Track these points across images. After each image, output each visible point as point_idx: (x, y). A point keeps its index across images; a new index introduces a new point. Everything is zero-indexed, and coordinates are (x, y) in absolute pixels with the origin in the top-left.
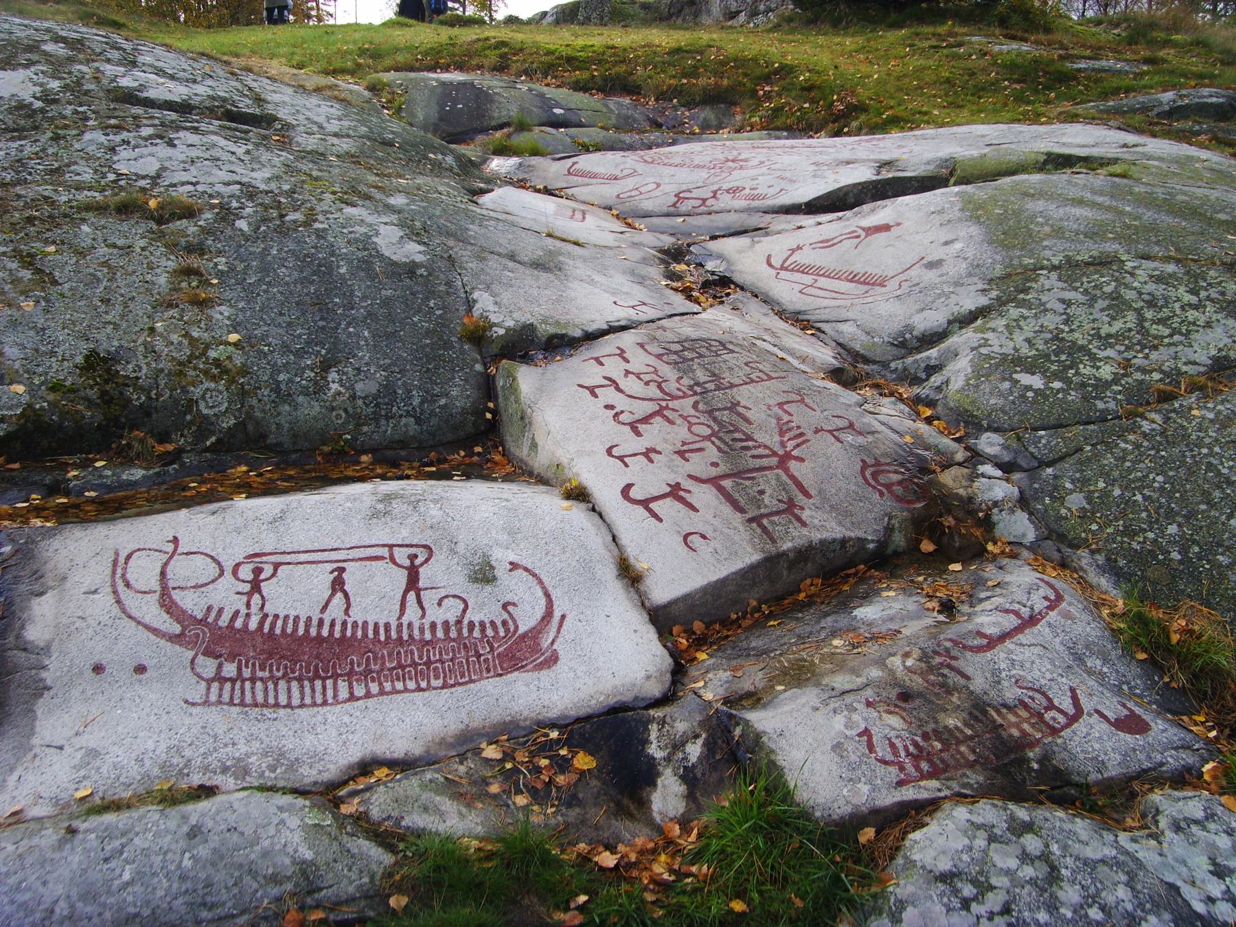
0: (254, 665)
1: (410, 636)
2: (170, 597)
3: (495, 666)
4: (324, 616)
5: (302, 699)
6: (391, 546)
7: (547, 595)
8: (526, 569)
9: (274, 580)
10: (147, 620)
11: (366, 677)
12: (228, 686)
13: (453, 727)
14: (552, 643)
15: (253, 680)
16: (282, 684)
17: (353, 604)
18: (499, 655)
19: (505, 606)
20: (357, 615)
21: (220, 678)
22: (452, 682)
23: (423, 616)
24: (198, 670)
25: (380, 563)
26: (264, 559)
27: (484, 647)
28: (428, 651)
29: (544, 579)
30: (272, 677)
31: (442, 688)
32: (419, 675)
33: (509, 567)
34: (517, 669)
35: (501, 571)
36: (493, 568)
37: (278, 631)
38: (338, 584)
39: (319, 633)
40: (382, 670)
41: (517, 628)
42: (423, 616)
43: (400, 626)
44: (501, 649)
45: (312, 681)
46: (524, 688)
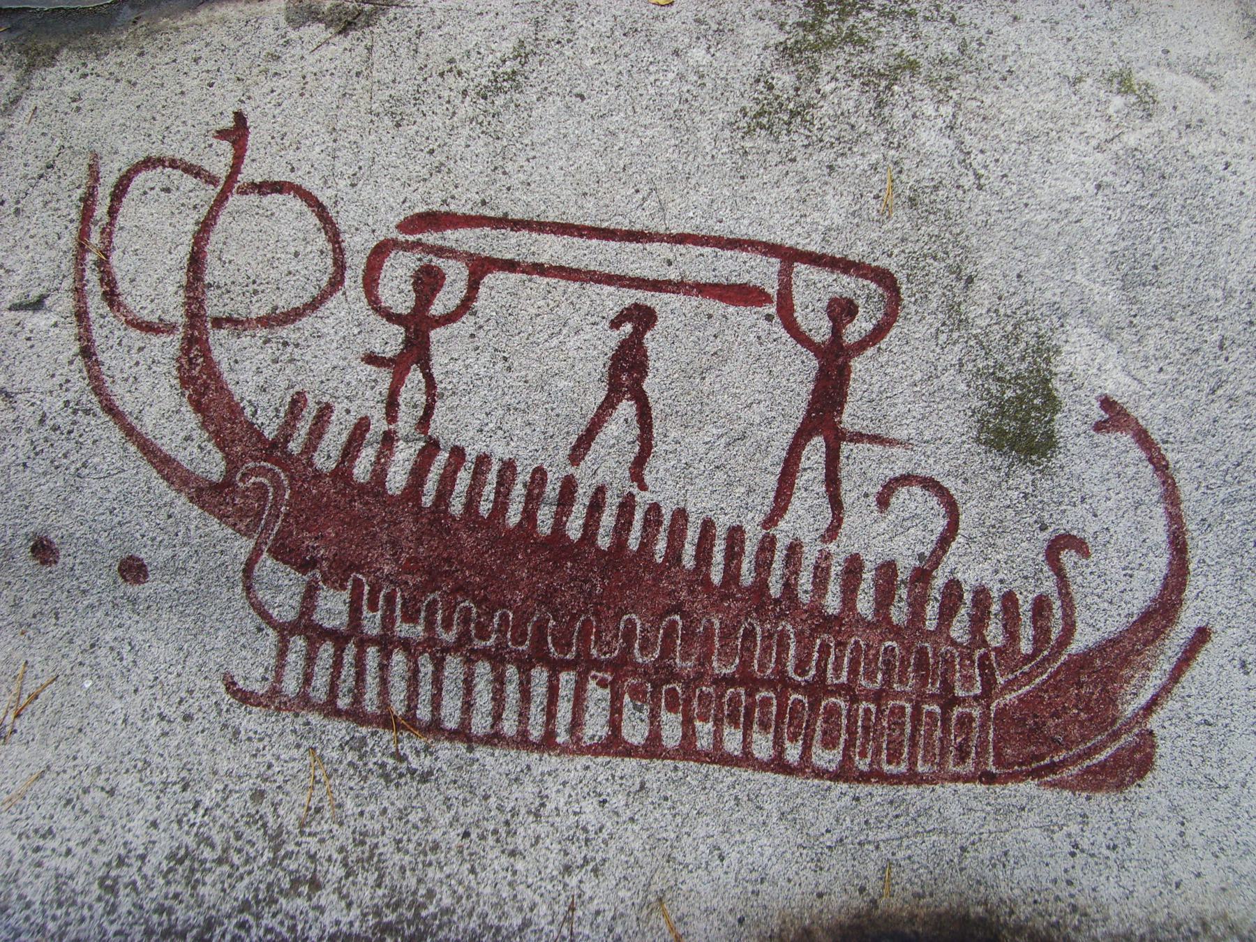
0: (390, 599)
1: (789, 587)
2: (206, 352)
3: (983, 744)
4: (577, 472)
5: (497, 717)
6: (789, 256)
7: (1178, 546)
8: (1143, 438)
9: (466, 324)
10: (148, 425)
11: (656, 687)
12: (326, 651)
13: (837, 900)
14: (1149, 708)
15: (386, 644)
16: (454, 667)
17: (659, 448)
18: (1001, 712)
19: (1053, 551)
20: (663, 487)
21: (305, 625)
22: (863, 765)
23: (832, 532)
24: (263, 595)
25: (747, 316)
26: (452, 237)
27: (968, 679)
28: (825, 649)
29: (1186, 489)
30: (430, 642)
31: (836, 777)
32: (789, 723)
33: (1098, 414)
34: (1036, 774)
35: (1072, 424)
36: (1051, 403)
37: (457, 506)
38: (627, 369)
39: (559, 526)
40: (699, 677)
41: (1069, 630)
42: (832, 532)
43: (767, 545)
44: (1010, 697)
45: (525, 667)
46: (1037, 837)
